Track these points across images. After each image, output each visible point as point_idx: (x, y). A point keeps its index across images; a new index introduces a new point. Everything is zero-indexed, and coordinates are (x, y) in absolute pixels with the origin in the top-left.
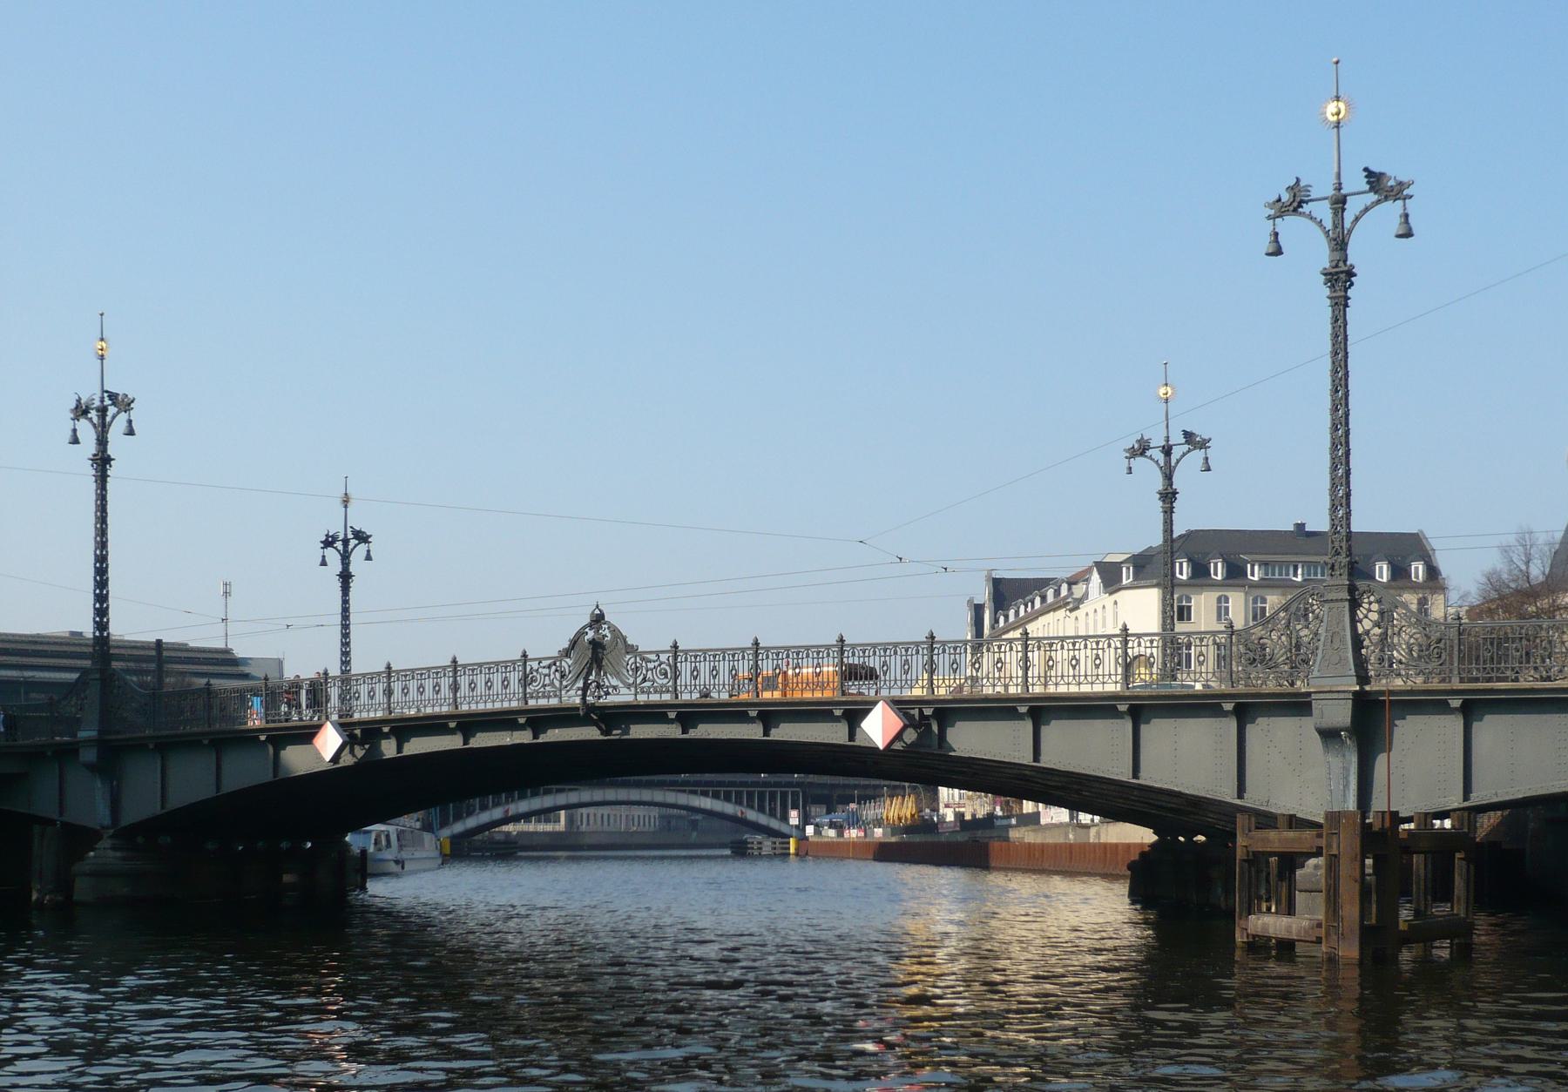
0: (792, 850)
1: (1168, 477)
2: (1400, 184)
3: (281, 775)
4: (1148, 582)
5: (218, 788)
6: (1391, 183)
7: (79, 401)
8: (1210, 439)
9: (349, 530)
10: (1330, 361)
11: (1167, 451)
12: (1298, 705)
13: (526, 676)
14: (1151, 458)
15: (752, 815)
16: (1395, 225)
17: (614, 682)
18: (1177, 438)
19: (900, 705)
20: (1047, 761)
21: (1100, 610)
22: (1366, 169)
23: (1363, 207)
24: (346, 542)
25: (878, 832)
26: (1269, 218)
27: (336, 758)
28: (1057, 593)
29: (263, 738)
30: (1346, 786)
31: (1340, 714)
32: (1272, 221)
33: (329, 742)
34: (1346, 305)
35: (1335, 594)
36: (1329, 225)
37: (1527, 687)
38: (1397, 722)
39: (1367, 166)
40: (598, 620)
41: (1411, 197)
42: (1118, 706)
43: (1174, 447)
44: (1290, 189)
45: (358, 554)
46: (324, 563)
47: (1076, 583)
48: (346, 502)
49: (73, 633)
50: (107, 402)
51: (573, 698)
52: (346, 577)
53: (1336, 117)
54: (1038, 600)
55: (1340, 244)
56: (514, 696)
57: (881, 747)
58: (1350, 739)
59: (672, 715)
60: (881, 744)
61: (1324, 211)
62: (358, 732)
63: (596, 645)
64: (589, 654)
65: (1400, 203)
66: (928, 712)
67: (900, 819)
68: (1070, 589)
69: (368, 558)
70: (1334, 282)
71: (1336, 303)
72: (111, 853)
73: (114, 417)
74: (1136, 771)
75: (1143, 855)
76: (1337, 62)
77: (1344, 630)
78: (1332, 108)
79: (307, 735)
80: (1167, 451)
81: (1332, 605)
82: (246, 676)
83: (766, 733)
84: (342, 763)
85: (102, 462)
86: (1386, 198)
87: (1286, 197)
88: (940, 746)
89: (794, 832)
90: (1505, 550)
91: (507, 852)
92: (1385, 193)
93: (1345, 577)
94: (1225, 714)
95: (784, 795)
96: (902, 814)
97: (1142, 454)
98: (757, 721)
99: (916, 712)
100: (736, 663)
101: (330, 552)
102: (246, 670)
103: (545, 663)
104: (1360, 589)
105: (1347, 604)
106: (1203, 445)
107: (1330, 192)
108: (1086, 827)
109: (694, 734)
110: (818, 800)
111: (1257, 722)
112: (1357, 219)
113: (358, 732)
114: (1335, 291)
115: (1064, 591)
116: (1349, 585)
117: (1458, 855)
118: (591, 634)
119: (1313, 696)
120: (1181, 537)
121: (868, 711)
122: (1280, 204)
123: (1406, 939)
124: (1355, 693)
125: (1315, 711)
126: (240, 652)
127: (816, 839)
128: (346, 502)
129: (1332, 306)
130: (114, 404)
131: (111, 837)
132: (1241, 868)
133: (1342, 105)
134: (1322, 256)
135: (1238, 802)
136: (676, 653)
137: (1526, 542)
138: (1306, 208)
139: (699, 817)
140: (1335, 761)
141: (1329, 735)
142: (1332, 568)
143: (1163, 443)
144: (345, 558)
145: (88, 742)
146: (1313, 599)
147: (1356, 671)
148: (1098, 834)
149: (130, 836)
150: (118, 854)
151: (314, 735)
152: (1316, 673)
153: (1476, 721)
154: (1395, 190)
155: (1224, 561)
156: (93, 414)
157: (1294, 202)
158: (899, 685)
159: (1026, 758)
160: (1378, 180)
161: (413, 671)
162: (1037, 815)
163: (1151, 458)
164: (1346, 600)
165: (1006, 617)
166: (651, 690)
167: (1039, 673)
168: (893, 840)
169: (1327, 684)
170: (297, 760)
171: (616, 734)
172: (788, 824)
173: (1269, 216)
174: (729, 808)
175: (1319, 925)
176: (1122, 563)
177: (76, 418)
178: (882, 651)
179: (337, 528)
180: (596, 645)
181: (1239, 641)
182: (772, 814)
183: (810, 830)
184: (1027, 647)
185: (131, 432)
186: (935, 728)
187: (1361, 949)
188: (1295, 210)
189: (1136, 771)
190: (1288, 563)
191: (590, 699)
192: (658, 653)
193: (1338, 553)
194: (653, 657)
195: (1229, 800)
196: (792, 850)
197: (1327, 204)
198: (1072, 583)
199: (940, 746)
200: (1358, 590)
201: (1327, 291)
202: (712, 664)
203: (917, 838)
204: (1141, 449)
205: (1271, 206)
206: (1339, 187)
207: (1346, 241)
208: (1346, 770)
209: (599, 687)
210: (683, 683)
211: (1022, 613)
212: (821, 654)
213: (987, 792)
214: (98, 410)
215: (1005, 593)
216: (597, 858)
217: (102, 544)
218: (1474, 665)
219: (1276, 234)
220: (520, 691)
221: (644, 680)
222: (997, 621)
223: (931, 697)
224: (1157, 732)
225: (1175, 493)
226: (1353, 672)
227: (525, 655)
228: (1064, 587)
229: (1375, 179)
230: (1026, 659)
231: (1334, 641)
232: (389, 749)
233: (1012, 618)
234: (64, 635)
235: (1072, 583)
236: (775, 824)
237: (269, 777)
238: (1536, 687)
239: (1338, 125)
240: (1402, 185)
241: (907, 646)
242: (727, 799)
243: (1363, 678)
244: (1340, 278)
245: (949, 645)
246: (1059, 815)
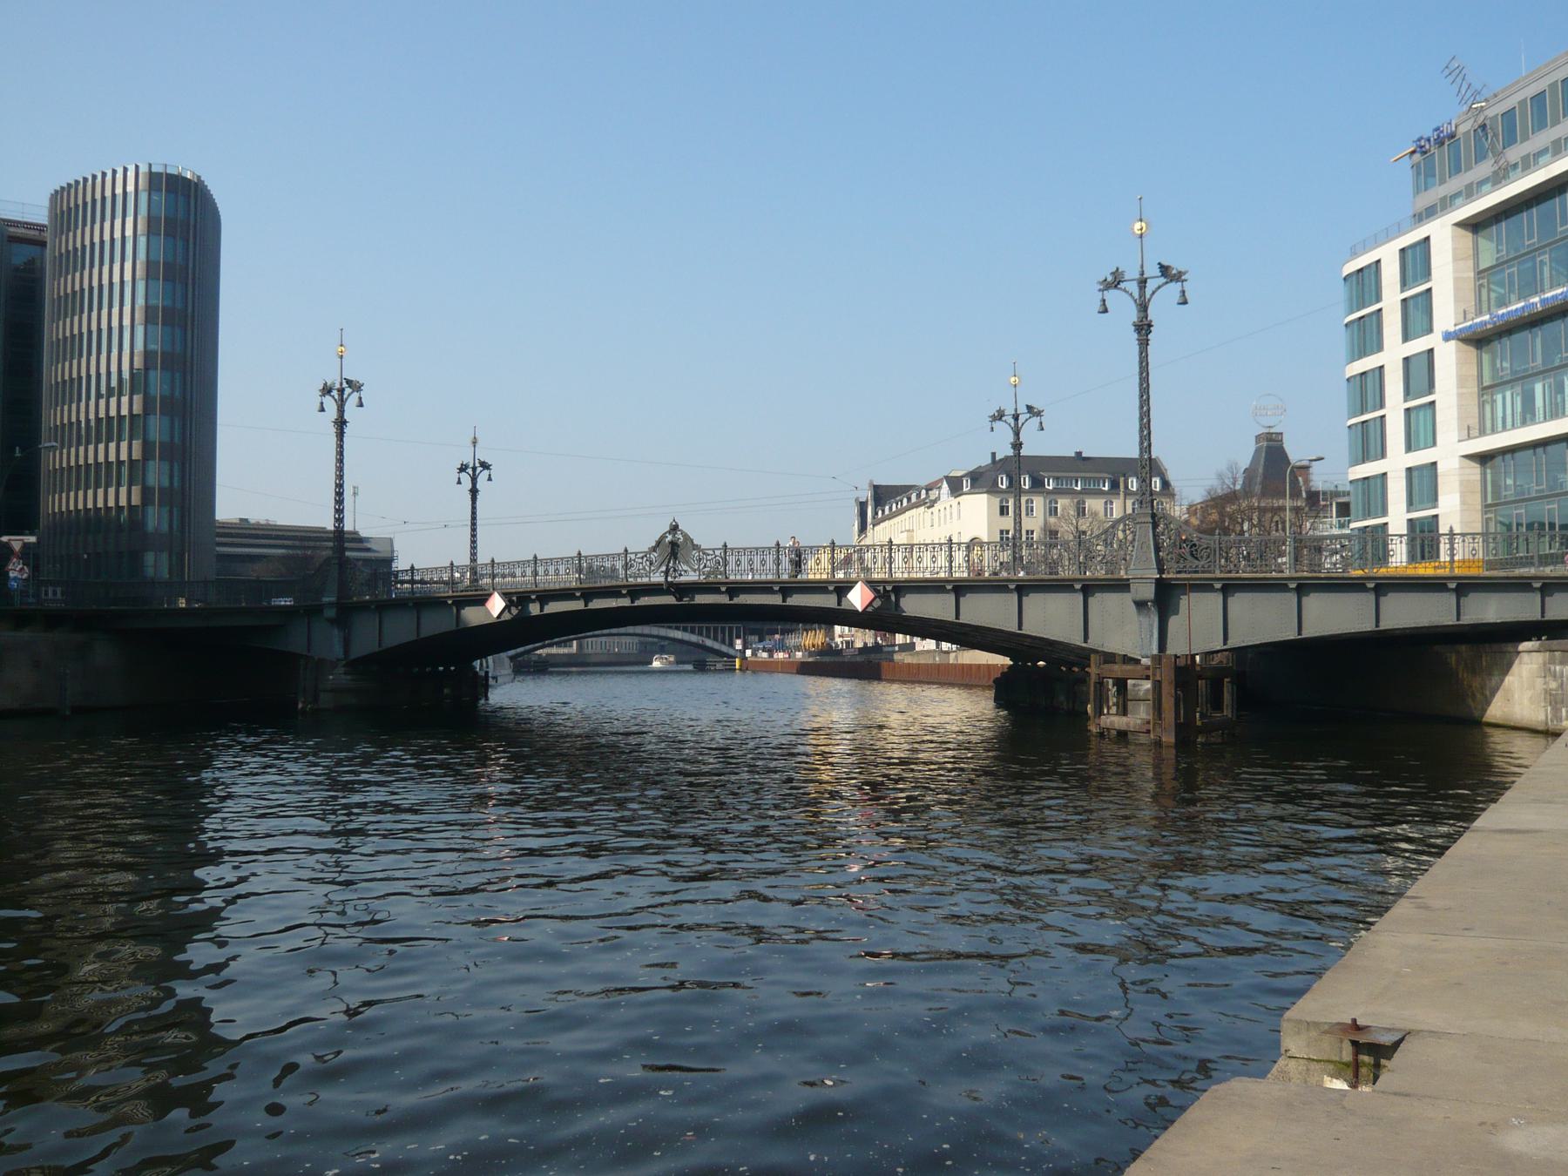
0: (737, 667)
1: (1017, 434)
2: (1180, 272)
3: (462, 626)
4: (981, 490)
5: (418, 634)
6: (1174, 272)
7: (325, 384)
9: (477, 461)
10: (1138, 377)
11: (1016, 417)
12: (1122, 586)
13: (627, 564)
14: (1005, 421)
15: (709, 643)
16: (1177, 297)
17: (685, 568)
18: (1022, 409)
19: (872, 584)
20: (963, 619)
21: (948, 508)
23: (1157, 286)
24: (474, 469)
25: (799, 655)
26: (1100, 290)
27: (499, 617)
28: (919, 496)
29: (450, 602)
30: (1152, 636)
31: (1148, 592)
33: (496, 605)
34: (1148, 344)
36: (1136, 295)
40: (674, 528)
44: (1112, 273)
45: (483, 476)
46: (459, 482)
47: (931, 489)
48: (475, 443)
49: (241, 520)
50: (345, 385)
51: (658, 578)
52: (474, 492)
54: (905, 500)
55: (1143, 307)
57: (860, 610)
59: (723, 589)
60: (860, 610)
61: (1133, 288)
62: (515, 598)
63: (674, 544)
64: (669, 550)
65: (1180, 284)
66: (889, 588)
67: (813, 646)
68: (927, 493)
69: (490, 479)
72: (343, 676)
73: (349, 395)
74: (1020, 626)
75: (1003, 674)
78: (1138, 226)
79: (481, 600)
80: (1016, 417)
82: (368, 550)
83: (784, 601)
84: (502, 619)
85: (341, 424)
86: (1171, 281)
87: (1110, 279)
88: (896, 610)
89: (738, 654)
90: (1220, 476)
91: (541, 668)
94: (1075, 591)
95: (731, 629)
96: (815, 643)
97: (1000, 419)
99: (881, 588)
101: (463, 475)
102: (369, 546)
103: (639, 555)
107: (1137, 276)
108: (947, 653)
109: (736, 601)
110: (753, 633)
112: (1154, 293)
113: (515, 598)
115: (923, 496)
117: (1226, 680)
118: (670, 538)
120: (1001, 460)
121: (851, 588)
123: (1200, 731)
124: (1156, 579)
126: (363, 534)
127: (754, 659)
128: (475, 443)
130: (350, 387)
131: (344, 666)
132: (1095, 687)
133: (1144, 225)
134: (1133, 315)
135: (1084, 645)
137: (1232, 468)
138: (1122, 285)
139: (666, 643)
140: (1145, 620)
141: (1140, 605)
142: (1141, 503)
143: (1013, 412)
144: (474, 480)
145: (330, 604)
148: (956, 657)
149: (357, 665)
150: (349, 677)
151: (486, 600)
152: (1132, 567)
155: (1030, 476)
156: (335, 393)
157: (1115, 281)
159: (951, 617)
161: (551, 559)
162: (912, 645)
163: (1005, 421)
165: (883, 511)
168: (811, 660)
169: (1139, 574)
170: (472, 616)
171: (686, 600)
172: (734, 648)
174: (694, 638)
175: (1148, 723)
176: (962, 477)
177: (323, 395)
179: (469, 460)
180: (674, 544)
182: (723, 642)
183: (748, 653)
184: (951, 548)
185: (361, 405)
186: (893, 598)
187: (1176, 736)
188: (1116, 286)
189: (1020, 626)
190: (1072, 478)
191: (670, 579)
192: (714, 550)
193: (1144, 494)
194: (711, 552)
195: (1078, 644)
196: (737, 667)
198: (928, 489)
199: (896, 610)
201: (1136, 336)
203: (827, 659)
204: (1000, 416)
205: (1101, 283)
208: (1151, 626)
209: (675, 570)
211: (894, 509)
213: (870, 629)
214: (338, 390)
215: (884, 496)
216: (601, 673)
217: (340, 476)
219: (1104, 301)
221: (705, 567)
222: (877, 514)
223: (890, 579)
224: (1033, 602)
225: (1021, 444)
227: (626, 550)
228: (924, 492)
229: (1165, 270)
230: (951, 556)
232: (534, 609)
233: (887, 512)
234: (234, 521)
235: (928, 489)
236: (724, 649)
237: (453, 627)
239: (1141, 236)
240: (1180, 274)
242: (693, 632)
243: (1161, 571)
244: (1143, 328)
246: (930, 644)
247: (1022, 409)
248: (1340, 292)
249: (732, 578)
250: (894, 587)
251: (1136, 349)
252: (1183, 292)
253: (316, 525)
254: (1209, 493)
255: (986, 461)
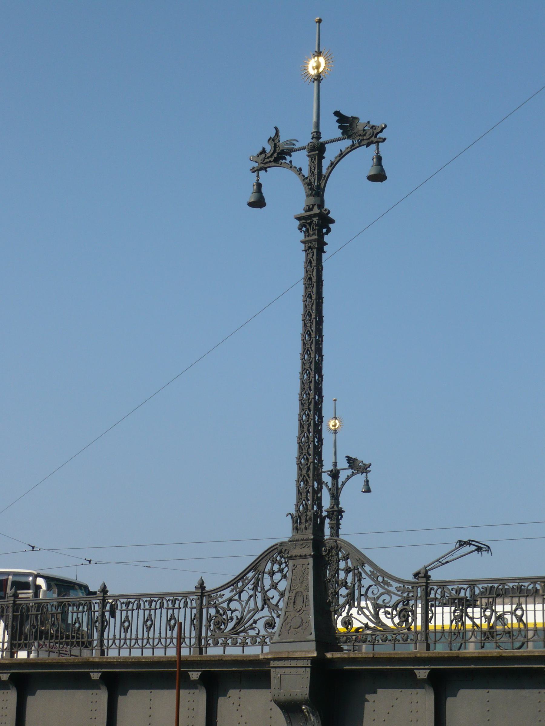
16: (371, 169)
35: (301, 550)
36: (306, 172)
37: (495, 655)
38: (368, 697)
41: (384, 139)
42: (91, 674)
53: (316, 71)
56: (136, 642)
58: (313, 715)
70: (308, 226)
71: (310, 248)
76: (320, 21)
77: (307, 589)
81: (297, 562)
87: (269, 149)
92: (358, 138)
93: (310, 531)
98: (199, 686)
100: (129, 613)
104: (328, 546)
105: (311, 561)
111: (228, 696)
114: (308, 236)
116: (313, 539)
119: (272, 664)
122: (263, 156)
124: (313, 660)
125: (274, 682)
129: (305, 251)
133: (322, 60)
136: (427, 587)
146: (282, 557)
147: (316, 636)
153: (221, 696)
154: (368, 134)
158: (140, 644)
160: (351, 125)
164: (310, 555)
166: (210, 642)
167: (115, 635)
169: (285, 649)
173: (254, 168)
178: (147, 604)
181: (209, 603)
197: (305, 152)
200: (325, 546)
202: (170, 611)
207: (322, 186)
210: (111, 636)
212: (131, 605)
218: (64, 640)
220: (193, 634)
226: (313, 637)
231: (297, 602)
238: (504, 655)
241: (174, 597)
245: (122, 601)
249: (113, 653)
250: (104, 675)
252: (379, 159)
253: (535, 576)
255: (337, 465)
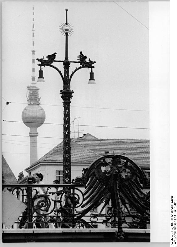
8: (95, 62)
11: (67, 64)
18: (73, 57)
22: (81, 53)
26: (39, 65)
32: (40, 66)
39: (82, 51)
43: (71, 63)
55: (67, 81)
61: (61, 67)
65: (90, 69)
80: (67, 64)
86: (83, 67)
106: (90, 65)
138: (53, 64)
206: (67, 58)
247: (73, 57)
248: (23, 203)
251: (63, 109)
254: (63, 231)
